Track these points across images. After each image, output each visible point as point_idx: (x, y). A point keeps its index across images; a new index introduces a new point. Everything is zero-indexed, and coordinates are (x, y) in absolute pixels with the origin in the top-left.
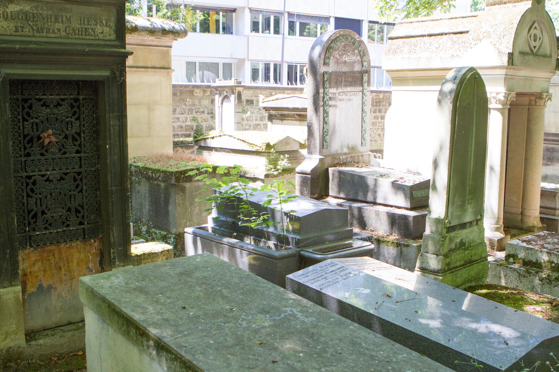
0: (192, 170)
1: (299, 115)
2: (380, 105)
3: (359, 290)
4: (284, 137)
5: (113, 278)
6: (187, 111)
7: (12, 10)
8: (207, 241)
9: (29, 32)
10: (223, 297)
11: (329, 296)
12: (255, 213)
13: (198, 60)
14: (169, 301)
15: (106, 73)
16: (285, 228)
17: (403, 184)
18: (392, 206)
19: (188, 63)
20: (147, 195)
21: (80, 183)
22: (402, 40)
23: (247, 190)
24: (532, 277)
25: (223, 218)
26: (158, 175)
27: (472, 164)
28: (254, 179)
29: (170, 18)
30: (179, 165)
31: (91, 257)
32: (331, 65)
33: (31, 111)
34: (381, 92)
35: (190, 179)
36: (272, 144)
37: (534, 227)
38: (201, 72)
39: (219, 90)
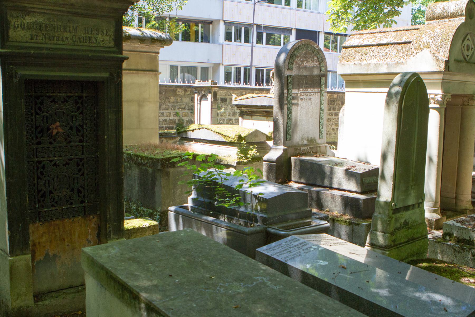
0: (176, 157)
1: (265, 112)
2: (334, 104)
3: (318, 262)
4: (254, 130)
5: (110, 249)
6: (171, 107)
7: (28, 21)
8: (186, 217)
9: (42, 40)
10: (204, 267)
11: (293, 267)
12: (229, 195)
13: (180, 64)
14: (158, 269)
15: (105, 75)
16: (254, 207)
17: (355, 171)
18: (345, 190)
19: (171, 67)
20: (137, 178)
21: (82, 167)
22: (355, 49)
23: (222, 176)
24: (465, 253)
25: (201, 199)
26: (146, 161)
27: (415, 155)
28: (228, 166)
29: (158, 29)
30: (164, 153)
31: (90, 231)
32: (294, 70)
33: (42, 107)
34: (335, 93)
35: (173, 165)
36: (243, 136)
37: (466, 209)
38: (182, 74)
39: (198, 90)
